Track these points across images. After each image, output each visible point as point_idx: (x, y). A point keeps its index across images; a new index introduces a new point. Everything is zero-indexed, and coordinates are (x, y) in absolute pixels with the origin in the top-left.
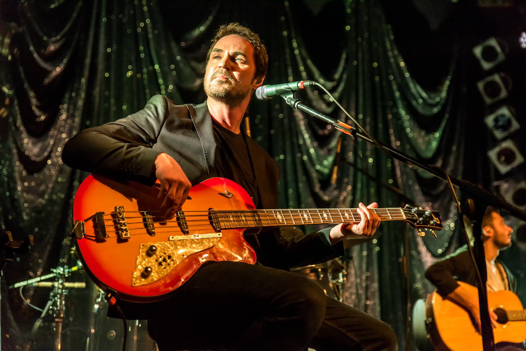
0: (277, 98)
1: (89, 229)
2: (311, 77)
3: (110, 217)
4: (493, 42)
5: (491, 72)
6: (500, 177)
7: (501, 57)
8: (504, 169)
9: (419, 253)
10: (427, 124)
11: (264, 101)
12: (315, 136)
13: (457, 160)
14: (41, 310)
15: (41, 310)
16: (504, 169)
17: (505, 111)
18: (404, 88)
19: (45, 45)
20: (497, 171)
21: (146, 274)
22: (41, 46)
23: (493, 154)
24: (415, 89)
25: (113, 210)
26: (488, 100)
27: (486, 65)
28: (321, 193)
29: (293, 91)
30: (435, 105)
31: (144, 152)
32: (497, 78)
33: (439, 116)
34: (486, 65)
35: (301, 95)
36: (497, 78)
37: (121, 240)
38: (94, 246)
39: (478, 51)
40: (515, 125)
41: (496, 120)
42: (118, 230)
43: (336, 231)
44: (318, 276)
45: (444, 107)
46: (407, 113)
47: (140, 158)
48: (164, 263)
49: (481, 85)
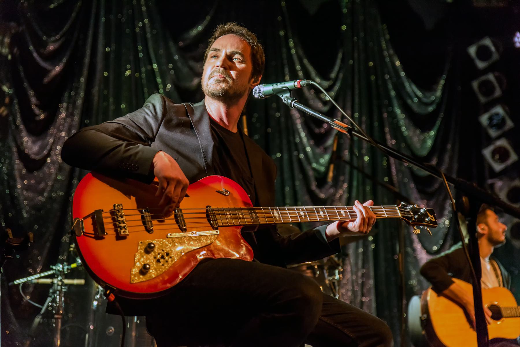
0: (274, 97)
1: (88, 226)
2: (307, 76)
3: (109, 215)
4: (487, 42)
5: (485, 71)
6: (494, 175)
7: (495, 56)
8: (498, 167)
9: (414, 250)
10: (422, 123)
11: (260, 100)
12: (311, 135)
13: (451, 158)
14: (40, 306)
15: (40, 306)
16: (498, 167)
17: (499, 110)
18: (399, 87)
19: (45, 45)
20: (491, 169)
21: (144, 270)
22: (40, 45)
23: (487, 152)
24: (411, 88)
25: (111, 207)
26: (482, 99)
27: (481, 65)
28: (317, 191)
29: (290, 90)
30: (431, 104)
31: (142, 151)
32: (491, 77)
33: (434, 115)
34: (481, 65)
35: (298, 94)
36: (491, 77)
37: (119, 237)
38: (93, 243)
39: (472, 50)
40: (510, 124)
41: (491, 119)
42: (117, 227)
43: (332, 229)
44: (314, 273)
45: (439, 106)
46: (402, 112)
47: (138, 156)
48: (162, 260)
49: (475, 84)
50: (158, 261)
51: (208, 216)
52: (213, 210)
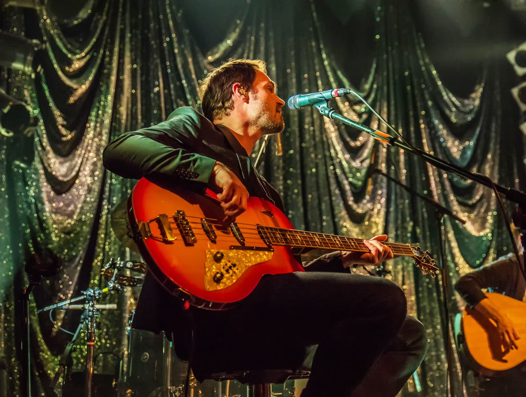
3: (172, 220)
10: (460, 132)
18: (436, 97)
19: (70, 63)
22: (65, 62)
24: (447, 96)
28: (355, 206)
39: (511, 56)
49: (515, 92)
50: (227, 271)
51: (260, 233)
52: (262, 228)
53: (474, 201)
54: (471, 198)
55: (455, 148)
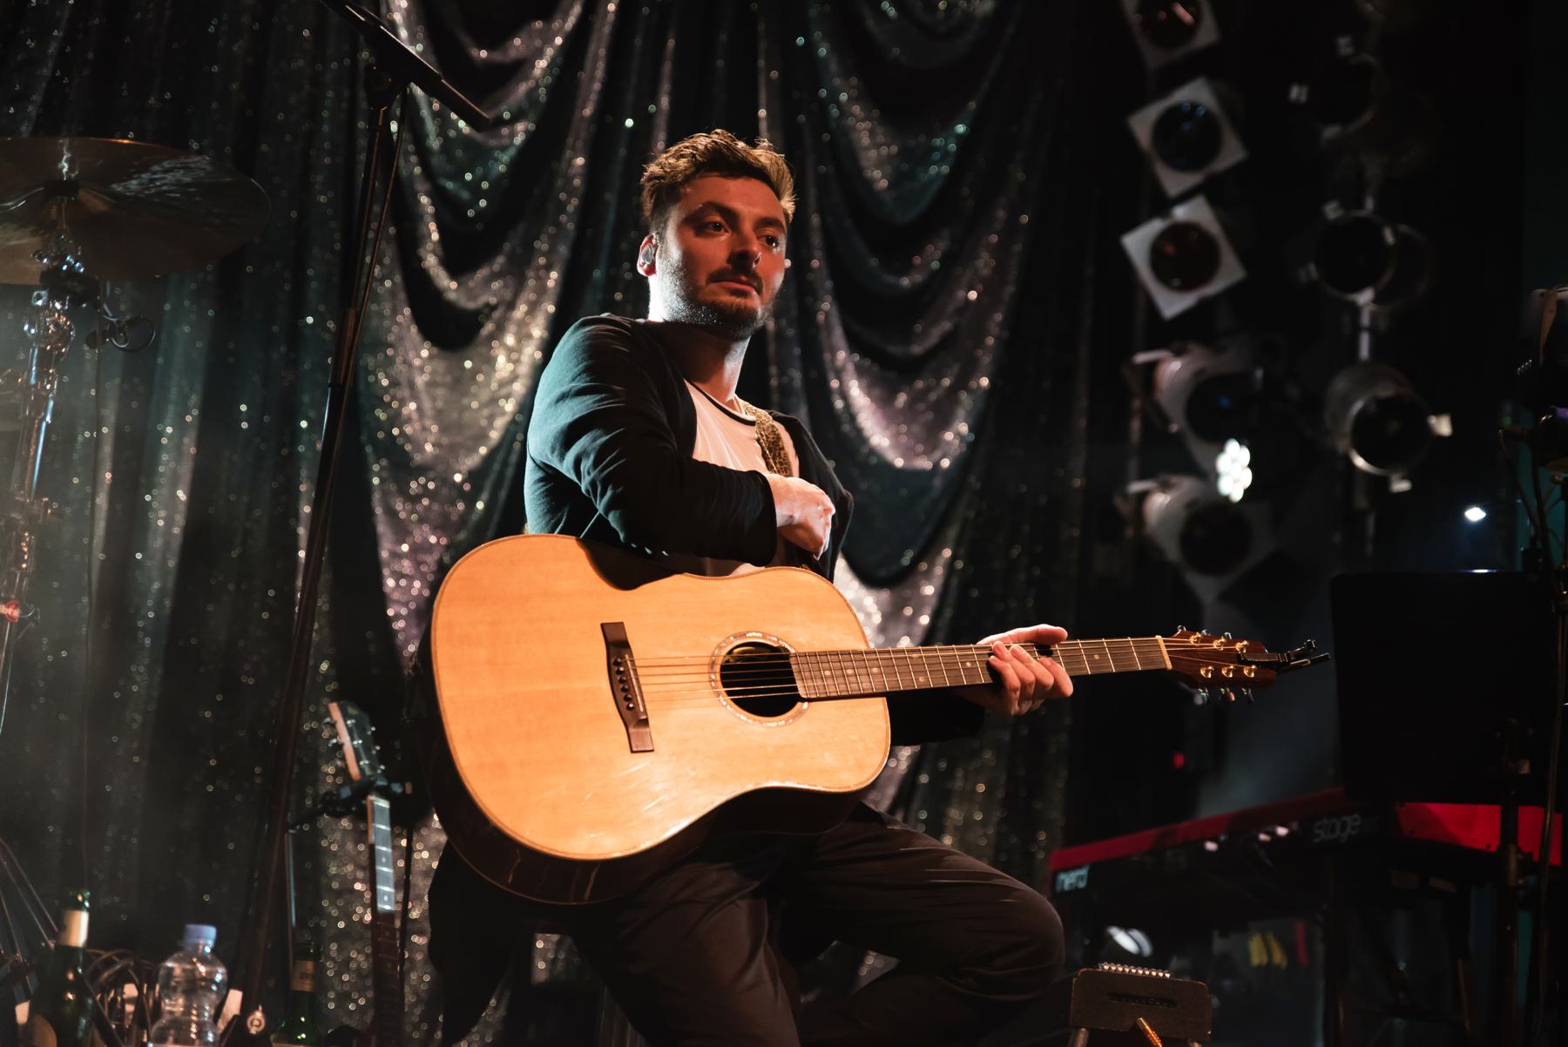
8: (1172, 304)
10: (904, 102)
17: (1196, 93)
20: (1152, 309)
23: (1137, 242)
26: (1153, 57)
28: (448, 284)
41: (1167, 125)
53: (917, 349)
54: (907, 337)
55: (874, 152)
